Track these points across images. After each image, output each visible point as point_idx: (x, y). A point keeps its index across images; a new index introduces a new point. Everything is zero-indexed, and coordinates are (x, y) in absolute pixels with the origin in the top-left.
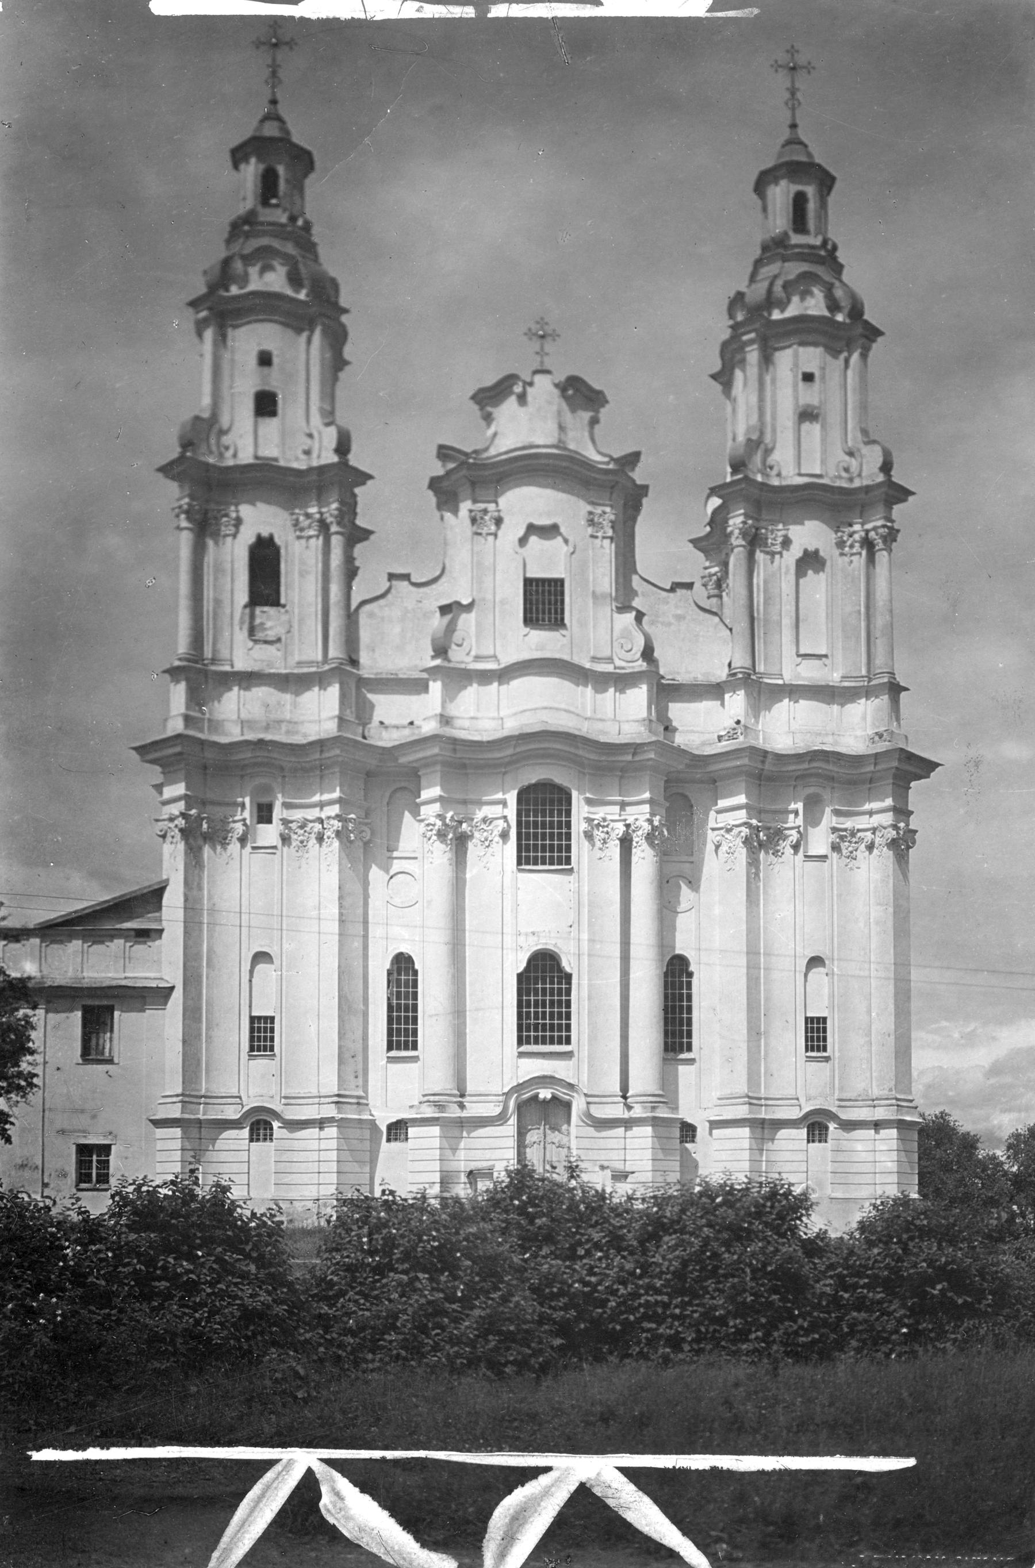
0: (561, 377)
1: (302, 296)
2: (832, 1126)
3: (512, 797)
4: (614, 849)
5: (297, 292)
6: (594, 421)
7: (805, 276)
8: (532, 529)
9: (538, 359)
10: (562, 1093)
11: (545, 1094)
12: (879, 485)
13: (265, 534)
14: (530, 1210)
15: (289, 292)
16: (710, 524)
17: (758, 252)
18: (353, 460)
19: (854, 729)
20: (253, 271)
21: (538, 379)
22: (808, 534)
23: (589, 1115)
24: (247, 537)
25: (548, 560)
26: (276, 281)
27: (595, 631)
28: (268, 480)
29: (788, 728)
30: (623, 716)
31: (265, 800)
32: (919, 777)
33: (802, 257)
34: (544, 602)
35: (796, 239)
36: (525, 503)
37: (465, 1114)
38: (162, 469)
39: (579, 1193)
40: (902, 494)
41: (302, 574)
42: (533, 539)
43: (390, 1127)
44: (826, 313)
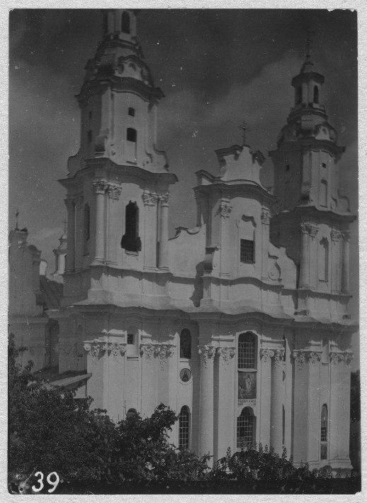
3: (236, 337)
4: (269, 361)
25: (247, 232)
30: (270, 303)
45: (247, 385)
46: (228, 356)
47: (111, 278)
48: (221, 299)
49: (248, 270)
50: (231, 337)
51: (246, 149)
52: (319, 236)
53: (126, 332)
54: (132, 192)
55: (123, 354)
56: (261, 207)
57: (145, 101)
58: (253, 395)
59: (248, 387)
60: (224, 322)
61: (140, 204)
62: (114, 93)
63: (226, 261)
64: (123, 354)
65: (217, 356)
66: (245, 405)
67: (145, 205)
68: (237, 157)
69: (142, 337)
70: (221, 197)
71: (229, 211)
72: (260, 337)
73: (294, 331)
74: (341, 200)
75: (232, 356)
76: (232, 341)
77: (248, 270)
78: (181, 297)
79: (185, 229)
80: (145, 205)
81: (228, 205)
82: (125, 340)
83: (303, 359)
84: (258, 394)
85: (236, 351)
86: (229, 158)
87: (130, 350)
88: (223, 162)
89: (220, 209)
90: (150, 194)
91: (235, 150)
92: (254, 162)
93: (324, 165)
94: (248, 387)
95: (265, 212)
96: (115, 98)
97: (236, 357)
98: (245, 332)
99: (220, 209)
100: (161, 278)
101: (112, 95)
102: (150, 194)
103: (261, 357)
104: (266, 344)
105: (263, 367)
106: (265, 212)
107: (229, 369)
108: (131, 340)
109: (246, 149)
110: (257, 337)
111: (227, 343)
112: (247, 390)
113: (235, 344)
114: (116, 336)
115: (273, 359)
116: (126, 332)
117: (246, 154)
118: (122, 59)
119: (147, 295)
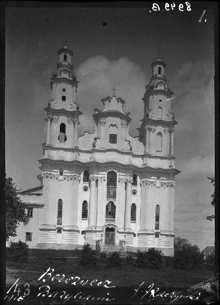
0: (117, 98)
1: (71, 79)
2: (159, 235)
3: (106, 173)
4: (124, 184)
5: (70, 78)
6: (123, 106)
7: (161, 82)
8: (112, 125)
9: (113, 94)
10: (114, 227)
11: (110, 227)
12: (172, 121)
13: (63, 122)
14: (81, 292)
15: (69, 78)
16: (146, 88)
17: (142, 143)
18: (79, 110)
19: (165, 165)
20: (62, 73)
21: (113, 97)
22: (160, 129)
23: (118, 231)
24: (60, 123)
25: (113, 131)
26: (65, 76)
27: (121, 145)
28: (63, 112)
29: (153, 163)
30: (124, 160)
31: (61, 171)
32: (177, 174)
33: (160, 79)
34: (113, 138)
35: (158, 75)
36: (111, 120)
37: (96, 230)
38: (44, 109)
39: (111, 257)
40: (175, 123)
41: (138, 213)
42: (111, 127)
43: (82, 232)
44: (164, 89)
45: (111, 192)
46: (103, 181)
47: (97, 153)
48: (101, 158)
49: (114, 146)
50: (104, 173)
51: (114, 98)
52: (157, 132)
53: (59, 170)
54: (63, 119)
55: (57, 179)
56: (121, 120)
57: (166, 96)
58: (114, 196)
59: (112, 193)
60: (99, 166)
61: (66, 124)
62: (57, 84)
63: (103, 143)
64: (57, 179)
65: (97, 181)
66: (110, 200)
67: (122, 127)
68: (110, 101)
69: (65, 172)
70: (101, 118)
71: (105, 123)
72: (118, 174)
73: (141, 172)
74: (170, 115)
75: (104, 180)
76: (105, 174)
77: (114, 146)
78: (84, 158)
79: (88, 132)
80: (69, 124)
81: (104, 121)
82: (59, 173)
83: (145, 184)
84: (117, 196)
85: (106, 179)
86: (107, 103)
87: (61, 178)
88: (104, 104)
89: (101, 123)
90: (71, 120)
91: (108, 99)
92: (118, 103)
93: (160, 101)
94: (112, 193)
95: (123, 122)
96: (57, 85)
97: (106, 181)
98: (111, 170)
99: (101, 123)
100: (75, 150)
101: (57, 85)
102: (71, 120)
103: (119, 181)
104: (120, 176)
105: (120, 187)
106: (123, 122)
107: (103, 186)
108: (61, 174)
109: (114, 98)
110: (116, 173)
111: (103, 175)
112: (112, 195)
113: (106, 176)
114: (56, 172)
115: (126, 184)
116: (59, 170)
117: (114, 100)
118: (61, 71)
119: (69, 157)
